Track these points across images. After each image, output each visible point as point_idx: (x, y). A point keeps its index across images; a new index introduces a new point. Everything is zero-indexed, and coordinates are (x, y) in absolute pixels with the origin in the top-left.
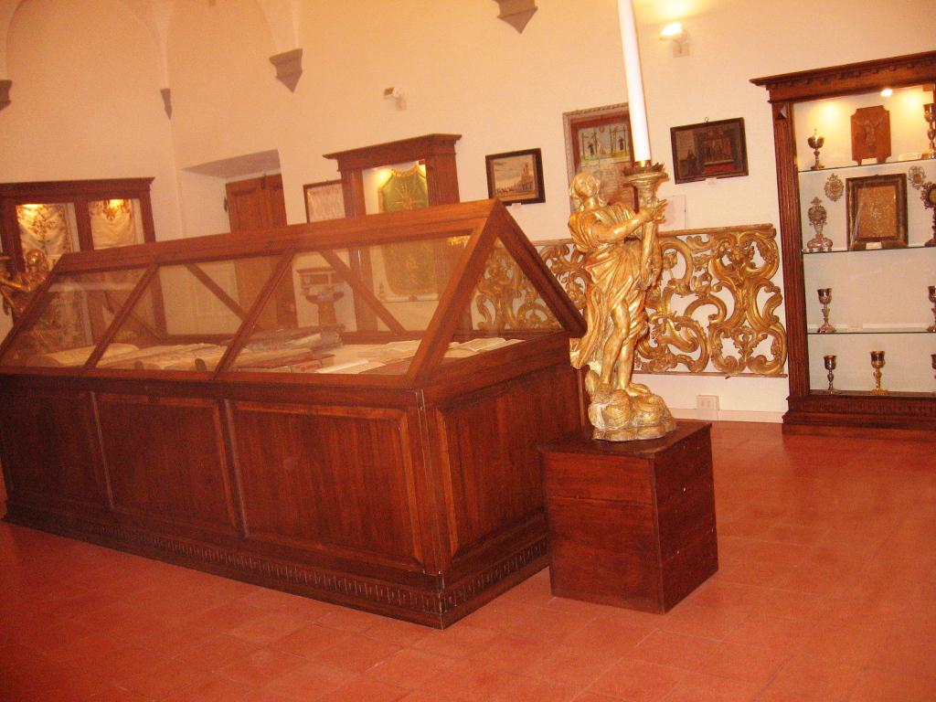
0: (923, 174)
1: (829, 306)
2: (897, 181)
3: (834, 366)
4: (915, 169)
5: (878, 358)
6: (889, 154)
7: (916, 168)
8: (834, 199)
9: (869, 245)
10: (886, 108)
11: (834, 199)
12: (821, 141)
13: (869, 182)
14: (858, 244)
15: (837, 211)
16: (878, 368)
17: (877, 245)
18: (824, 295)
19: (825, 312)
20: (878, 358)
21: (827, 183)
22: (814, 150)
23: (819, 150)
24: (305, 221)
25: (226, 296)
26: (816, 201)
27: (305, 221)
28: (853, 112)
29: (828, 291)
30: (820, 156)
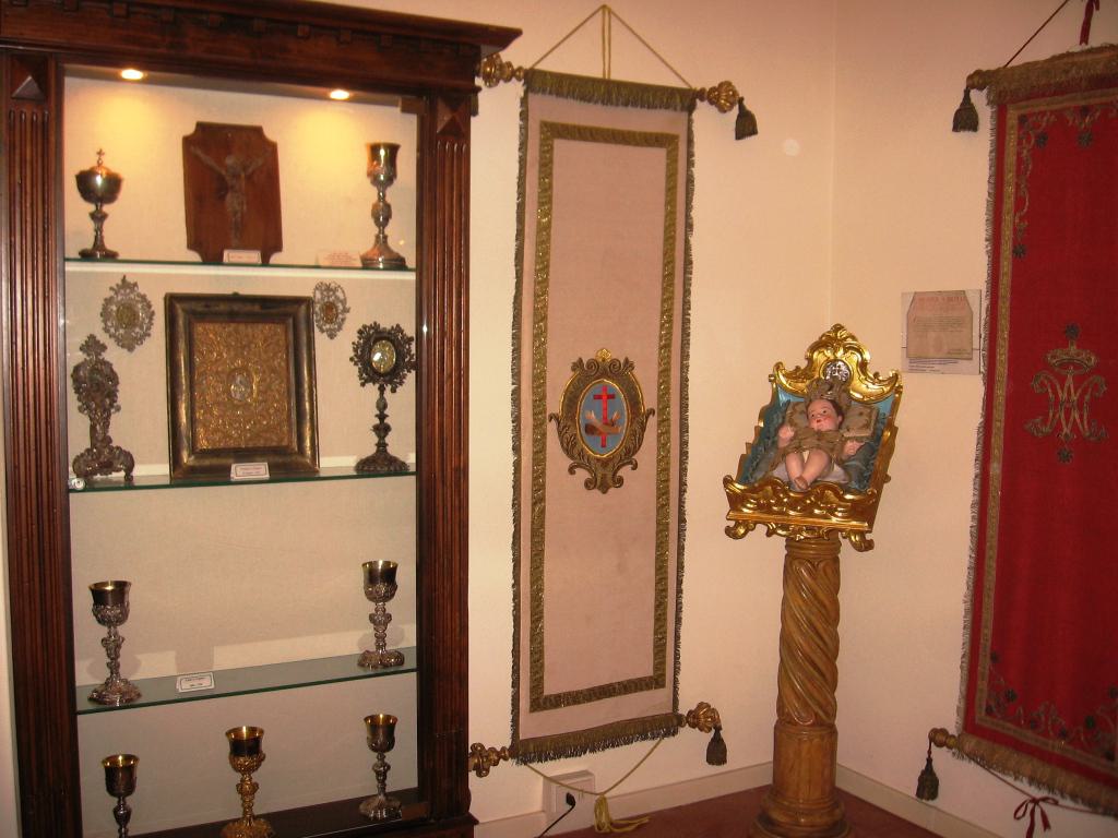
0: (344, 302)
1: (122, 630)
2: (289, 318)
3: (130, 788)
4: (327, 289)
5: (246, 748)
6: (278, 247)
7: (328, 288)
8: (129, 344)
9: (239, 471)
10: (270, 134)
11: (129, 344)
12: (114, 183)
13: (222, 307)
14: (198, 469)
15: (142, 374)
16: (248, 770)
17: (260, 470)
18: (112, 600)
19: (113, 648)
20: (246, 748)
21: (108, 301)
22: (92, 208)
23: (106, 208)
24: (415, 673)
25: (985, 534)
26: (92, 346)
27: (415, 673)
28: (190, 129)
29: (121, 587)
30: (107, 224)
